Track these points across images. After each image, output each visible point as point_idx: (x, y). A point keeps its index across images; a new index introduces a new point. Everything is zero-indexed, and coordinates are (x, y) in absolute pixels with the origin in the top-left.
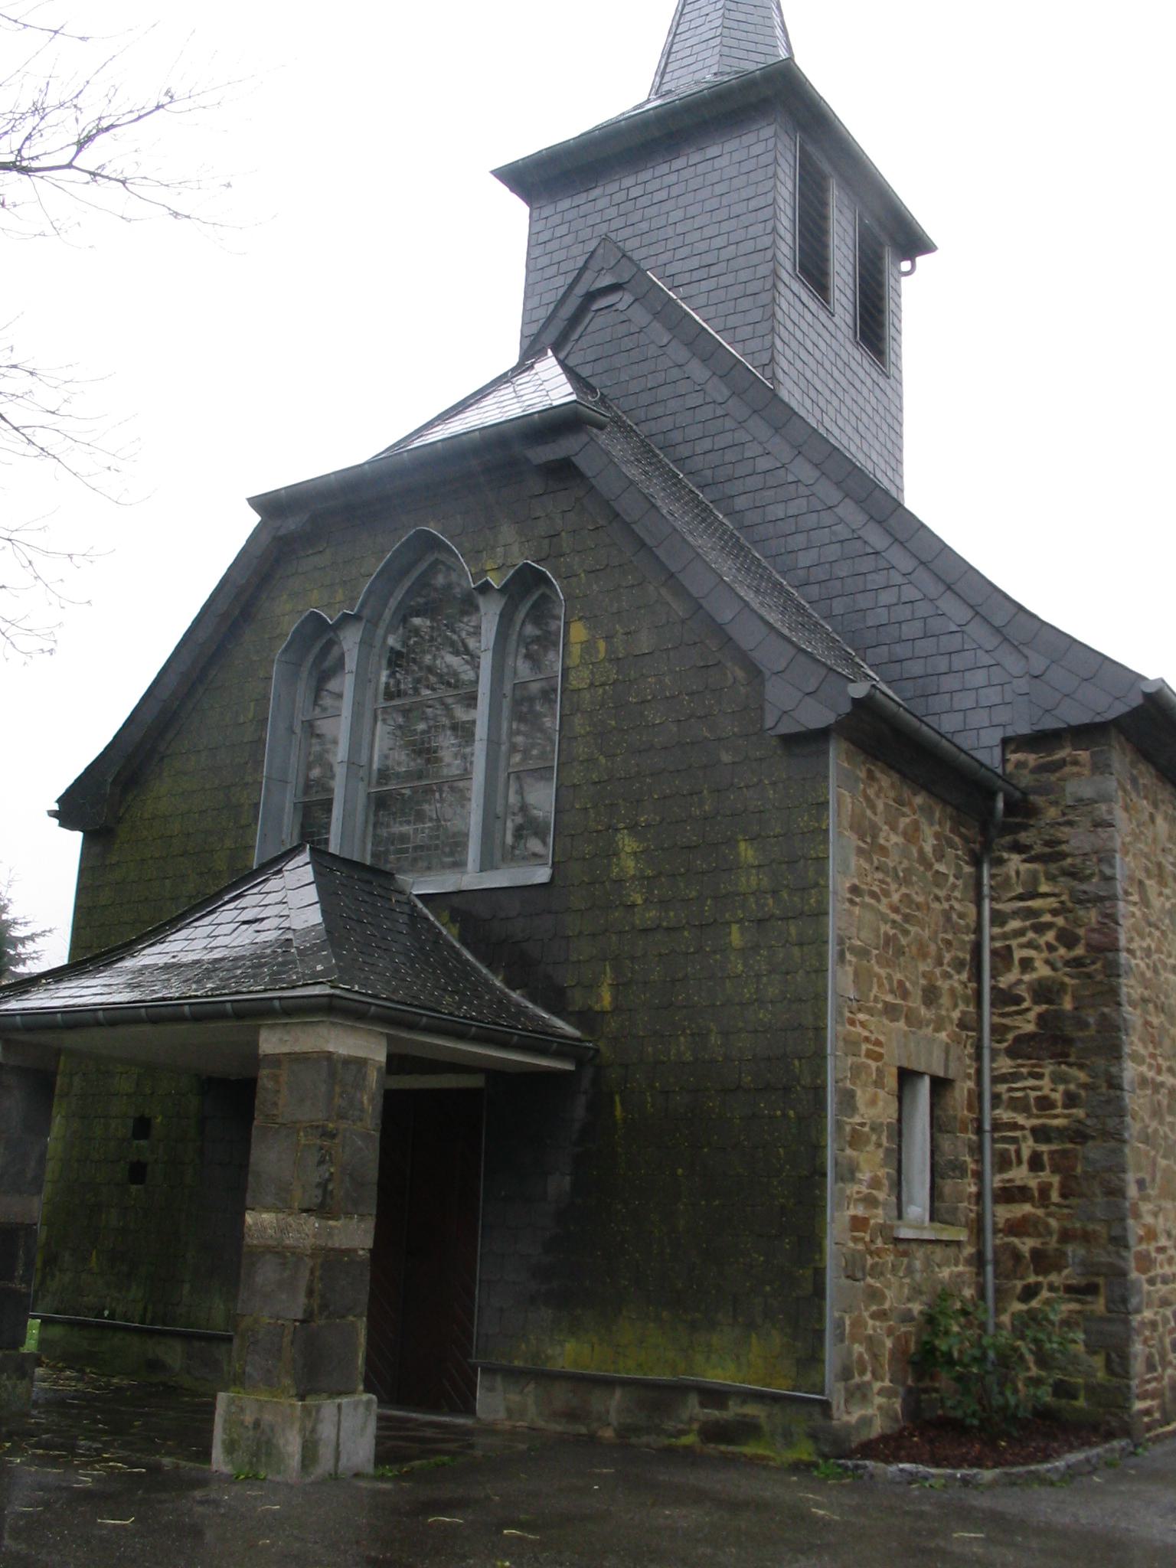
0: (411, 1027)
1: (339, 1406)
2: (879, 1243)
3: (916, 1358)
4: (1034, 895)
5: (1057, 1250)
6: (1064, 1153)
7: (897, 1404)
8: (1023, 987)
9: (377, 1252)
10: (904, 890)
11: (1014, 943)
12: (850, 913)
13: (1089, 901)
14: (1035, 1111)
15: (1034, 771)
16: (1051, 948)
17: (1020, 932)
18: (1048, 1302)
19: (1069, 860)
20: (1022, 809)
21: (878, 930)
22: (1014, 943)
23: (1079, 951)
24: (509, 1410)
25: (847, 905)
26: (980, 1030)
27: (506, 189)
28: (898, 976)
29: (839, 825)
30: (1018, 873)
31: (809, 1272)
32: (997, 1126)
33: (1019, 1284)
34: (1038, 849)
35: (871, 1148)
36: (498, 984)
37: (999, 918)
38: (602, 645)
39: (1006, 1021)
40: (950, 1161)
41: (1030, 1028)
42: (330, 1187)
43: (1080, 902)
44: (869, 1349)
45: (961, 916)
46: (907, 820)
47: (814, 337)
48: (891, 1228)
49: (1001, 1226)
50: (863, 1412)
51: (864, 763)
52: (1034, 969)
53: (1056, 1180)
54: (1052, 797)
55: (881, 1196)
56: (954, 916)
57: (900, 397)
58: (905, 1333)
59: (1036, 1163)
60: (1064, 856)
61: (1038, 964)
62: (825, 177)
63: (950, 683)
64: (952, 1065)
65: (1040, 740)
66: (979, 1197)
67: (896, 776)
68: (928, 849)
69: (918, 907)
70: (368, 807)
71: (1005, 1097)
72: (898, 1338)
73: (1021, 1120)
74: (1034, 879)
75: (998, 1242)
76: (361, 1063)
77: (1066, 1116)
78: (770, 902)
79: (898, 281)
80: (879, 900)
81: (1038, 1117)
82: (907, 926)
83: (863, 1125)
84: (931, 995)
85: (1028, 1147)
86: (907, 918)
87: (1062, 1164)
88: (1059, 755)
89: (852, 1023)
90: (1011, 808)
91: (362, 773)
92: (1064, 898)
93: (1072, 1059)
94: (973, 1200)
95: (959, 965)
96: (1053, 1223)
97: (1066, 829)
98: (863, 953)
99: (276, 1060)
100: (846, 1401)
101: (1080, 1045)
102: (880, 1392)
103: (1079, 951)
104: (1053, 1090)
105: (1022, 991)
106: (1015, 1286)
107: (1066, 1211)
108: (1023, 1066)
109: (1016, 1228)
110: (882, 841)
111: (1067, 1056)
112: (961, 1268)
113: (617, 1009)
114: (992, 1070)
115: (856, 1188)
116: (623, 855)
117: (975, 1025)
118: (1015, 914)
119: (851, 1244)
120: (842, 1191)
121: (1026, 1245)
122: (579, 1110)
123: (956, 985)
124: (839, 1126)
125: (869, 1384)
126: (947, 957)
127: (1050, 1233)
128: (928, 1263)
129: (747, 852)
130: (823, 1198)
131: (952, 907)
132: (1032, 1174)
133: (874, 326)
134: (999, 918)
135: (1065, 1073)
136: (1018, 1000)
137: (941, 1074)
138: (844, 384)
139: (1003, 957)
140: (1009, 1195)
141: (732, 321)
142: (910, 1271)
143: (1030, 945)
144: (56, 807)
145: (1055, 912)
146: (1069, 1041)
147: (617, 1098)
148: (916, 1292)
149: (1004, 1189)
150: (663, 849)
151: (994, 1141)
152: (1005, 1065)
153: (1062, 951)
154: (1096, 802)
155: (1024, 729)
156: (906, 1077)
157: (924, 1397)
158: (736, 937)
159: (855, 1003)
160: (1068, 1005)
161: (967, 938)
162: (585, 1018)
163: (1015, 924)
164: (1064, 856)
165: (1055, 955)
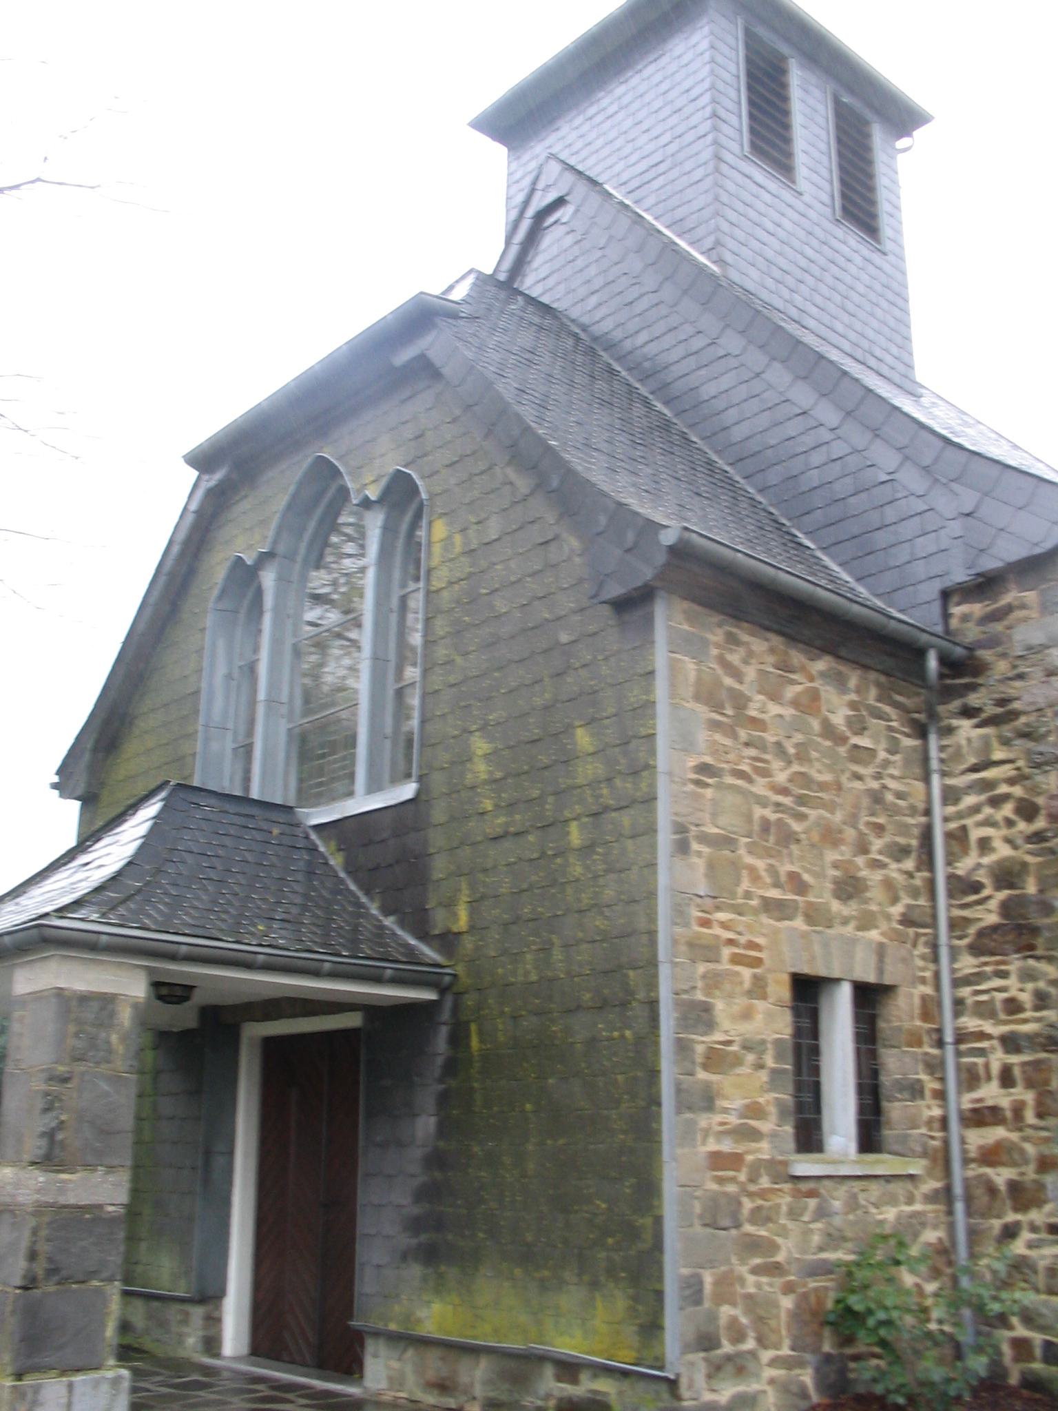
0: (173, 957)
1: (70, 1386)
2: (765, 1182)
3: (832, 1318)
4: (989, 764)
5: (1035, 1181)
6: (1036, 1064)
7: (807, 1377)
8: (982, 872)
10: (796, 768)
11: (969, 822)
12: (696, 797)
13: (1046, 763)
14: (1003, 1016)
16: (1010, 823)
17: (976, 809)
18: (1030, 1246)
19: (1023, 719)
20: (963, 668)
21: (749, 818)
22: (969, 822)
23: (1040, 823)
24: (390, 1379)
25: (691, 787)
26: (934, 924)
27: (489, 140)
28: (785, 868)
29: (673, 694)
30: (969, 740)
31: (648, 1221)
32: (961, 1037)
33: (996, 1224)
34: (991, 710)
35: (745, 1070)
36: (374, 912)
37: (951, 795)
38: (458, 539)
39: (966, 913)
40: (897, 1081)
41: (993, 919)
42: (60, 1136)
43: (1038, 766)
44: (749, 1311)
45: (900, 795)
46: (798, 688)
47: (776, 216)
48: (785, 1164)
49: (972, 1155)
50: (741, 1388)
51: (720, 625)
52: (993, 850)
54: (1000, 649)
55: (765, 1126)
56: (889, 797)
57: (904, 273)
58: (816, 1290)
59: (1007, 1079)
60: (1015, 714)
61: (997, 844)
62: (784, 59)
63: (882, 539)
64: (889, 968)
65: (985, 585)
66: (944, 1122)
67: (777, 640)
68: (839, 719)
69: (822, 786)
70: (289, 743)
71: (970, 1001)
72: (805, 1296)
73: (988, 1027)
74: (986, 746)
75: (970, 1173)
76: (107, 1001)
77: (1038, 1020)
78: (605, 791)
79: (893, 158)
80: (750, 780)
81: (1005, 1023)
82: (803, 809)
83: (729, 1043)
84: (849, 888)
85: (998, 1058)
86: (802, 800)
87: (1036, 1077)
89: (706, 923)
90: (952, 666)
91: (284, 710)
92: (1021, 763)
93: (1039, 952)
94: (936, 1125)
95: (901, 852)
96: (1030, 1149)
97: (1018, 684)
98: (727, 842)
99: (24, 1001)
100: (709, 1377)
101: (1047, 934)
102: (774, 1362)
103: (1040, 823)
104: (1021, 990)
105: (982, 877)
106: (991, 1228)
107: (1045, 1134)
108: (986, 964)
109: (991, 1156)
110: (753, 713)
111: (1032, 947)
112: (918, 1207)
113: (472, 928)
114: (953, 971)
115: (718, 1118)
116: (476, 760)
117: (928, 920)
118: (970, 788)
119: (714, 1186)
120: (691, 1124)
121: (1001, 1176)
122: (441, 1043)
123: (895, 875)
124: (683, 1047)
125: (753, 1354)
126: (877, 844)
127: (1026, 1162)
128: (853, 1204)
129: (583, 739)
130: (658, 1132)
131: (885, 787)
132: (1003, 1091)
133: (860, 204)
134: (951, 795)
135: (1034, 969)
136: (976, 887)
137: (871, 978)
138: (822, 261)
139: (958, 838)
140: (981, 1117)
141: (679, 213)
142: (822, 1213)
144: (56, 779)
145: (1011, 781)
146: (1035, 931)
147: (473, 1027)
148: (833, 1239)
149: (974, 1110)
150: (510, 747)
151: (959, 1054)
152: (968, 964)
153: (1022, 826)
154: (1048, 647)
155: (960, 576)
156: (808, 991)
157: (852, 1365)
158: (576, 836)
159: (708, 901)
160: (1031, 888)
161: (911, 821)
162: (447, 941)
163: (970, 800)
164: (1015, 714)
165: (1014, 830)
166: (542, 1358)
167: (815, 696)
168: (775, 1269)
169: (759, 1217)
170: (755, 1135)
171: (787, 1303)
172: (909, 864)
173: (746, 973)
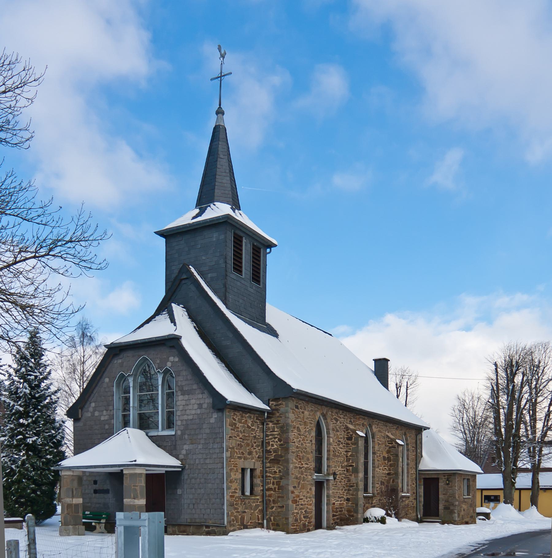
9: (146, 505)
15: (275, 406)
17: (271, 439)
23: (282, 442)
28: (241, 451)
34: (275, 422)
41: (273, 458)
45: (259, 436)
53: (277, 487)
59: (273, 484)
69: (247, 437)
87: (278, 483)
88: (280, 402)
95: (258, 446)
98: (233, 448)
99: (126, 474)
103: (282, 442)
105: (271, 450)
118: (271, 435)
126: (255, 445)
137: (253, 468)
143: (273, 441)
145: (278, 435)
152: (268, 465)
156: (243, 470)
163: (270, 437)
166: (202, 526)
167: (246, 420)
168: (238, 512)
169: (236, 504)
170: (236, 493)
171: (240, 517)
172: (260, 448)
173: (235, 468)
